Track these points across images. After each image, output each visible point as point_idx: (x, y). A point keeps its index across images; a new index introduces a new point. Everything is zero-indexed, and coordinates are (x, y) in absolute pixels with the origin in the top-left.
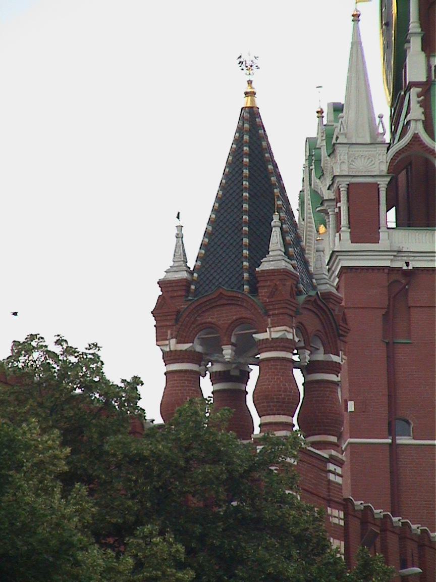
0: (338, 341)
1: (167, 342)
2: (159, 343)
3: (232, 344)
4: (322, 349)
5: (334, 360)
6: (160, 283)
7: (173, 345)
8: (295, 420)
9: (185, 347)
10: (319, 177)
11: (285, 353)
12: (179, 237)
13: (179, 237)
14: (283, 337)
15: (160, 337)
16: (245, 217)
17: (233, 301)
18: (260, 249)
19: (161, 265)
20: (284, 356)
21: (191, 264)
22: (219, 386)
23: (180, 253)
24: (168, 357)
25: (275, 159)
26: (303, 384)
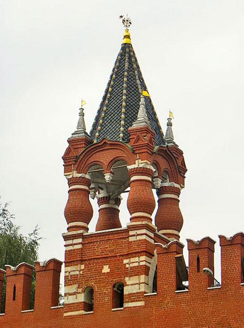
0: (179, 175)
1: (71, 173)
2: (65, 174)
3: (111, 172)
4: (168, 180)
5: (175, 186)
6: (69, 141)
7: (76, 175)
8: (153, 217)
9: (80, 175)
10: (190, 248)
11: (147, 177)
12: (82, 115)
13: (82, 115)
14: (145, 167)
15: (67, 168)
16: (124, 97)
17: (115, 145)
18: (132, 117)
19: (70, 129)
20: (143, 215)
21: (88, 131)
22: (116, 207)
23: (82, 123)
24: (71, 182)
25: (98, 217)
26: (158, 202)
